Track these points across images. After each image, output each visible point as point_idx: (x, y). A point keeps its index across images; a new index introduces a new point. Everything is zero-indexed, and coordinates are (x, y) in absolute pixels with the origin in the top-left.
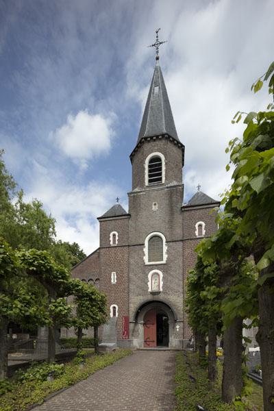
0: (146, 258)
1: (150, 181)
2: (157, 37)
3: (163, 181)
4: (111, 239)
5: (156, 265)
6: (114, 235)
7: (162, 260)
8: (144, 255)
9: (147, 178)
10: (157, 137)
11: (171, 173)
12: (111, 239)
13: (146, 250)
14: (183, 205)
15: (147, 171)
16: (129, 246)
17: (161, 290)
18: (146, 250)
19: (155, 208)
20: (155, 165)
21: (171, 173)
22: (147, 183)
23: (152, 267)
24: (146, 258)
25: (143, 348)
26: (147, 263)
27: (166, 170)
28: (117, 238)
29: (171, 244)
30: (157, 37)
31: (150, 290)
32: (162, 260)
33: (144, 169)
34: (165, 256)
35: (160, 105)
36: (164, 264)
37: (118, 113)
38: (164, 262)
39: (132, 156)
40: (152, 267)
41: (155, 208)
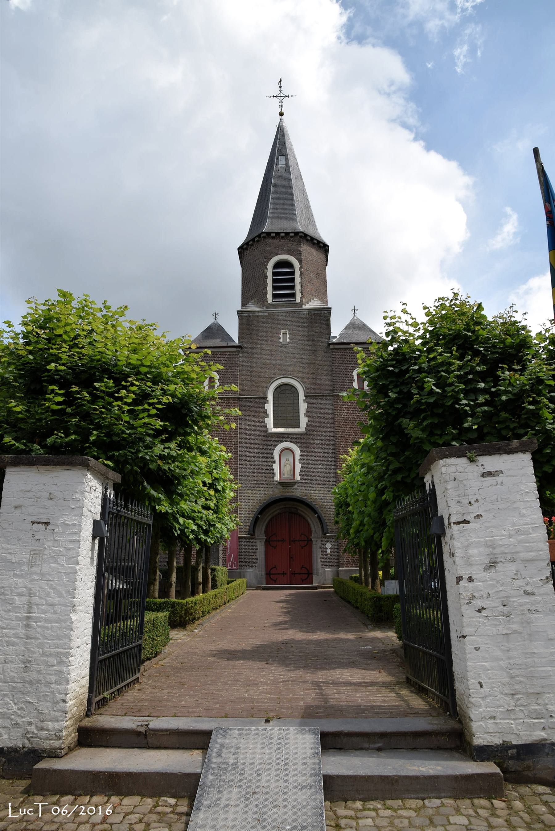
1: (275, 296)
7: (298, 426)
8: (267, 415)
10: (287, 234)
13: (270, 407)
16: (239, 398)
17: (298, 478)
18: (270, 407)
20: (284, 278)
23: (282, 437)
24: (270, 421)
29: (313, 400)
30: (281, 87)
31: (277, 478)
32: (298, 426)
33: (266, 277)
34: (304, 421)
36: (302, 434)
38: (301, 429)
40: (282, 437)
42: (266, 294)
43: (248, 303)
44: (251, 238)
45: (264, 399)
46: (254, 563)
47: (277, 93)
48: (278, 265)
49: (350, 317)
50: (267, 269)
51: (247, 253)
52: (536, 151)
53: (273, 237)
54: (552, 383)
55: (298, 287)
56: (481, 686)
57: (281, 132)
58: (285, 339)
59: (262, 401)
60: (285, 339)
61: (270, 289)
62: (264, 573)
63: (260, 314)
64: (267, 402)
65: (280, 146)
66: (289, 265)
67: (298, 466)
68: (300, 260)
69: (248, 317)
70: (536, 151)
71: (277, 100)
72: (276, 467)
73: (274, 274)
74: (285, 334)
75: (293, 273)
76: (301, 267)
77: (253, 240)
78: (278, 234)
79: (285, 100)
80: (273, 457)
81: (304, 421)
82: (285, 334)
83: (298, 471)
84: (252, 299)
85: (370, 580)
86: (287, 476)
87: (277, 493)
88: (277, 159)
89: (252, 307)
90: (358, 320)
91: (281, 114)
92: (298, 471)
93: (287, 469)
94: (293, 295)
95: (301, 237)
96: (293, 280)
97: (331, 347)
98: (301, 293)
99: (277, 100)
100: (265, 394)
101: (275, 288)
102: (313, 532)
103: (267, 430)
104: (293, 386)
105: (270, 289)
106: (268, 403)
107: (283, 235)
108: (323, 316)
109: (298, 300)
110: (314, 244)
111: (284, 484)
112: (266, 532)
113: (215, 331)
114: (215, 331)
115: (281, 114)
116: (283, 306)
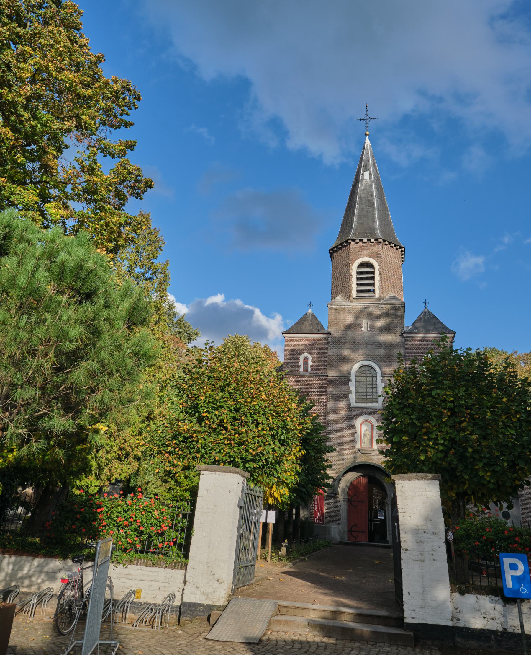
0: (352, 397)
2: (367, 111)
3: (377, 294)
4: (301, 363)
5: (368, 409)
6: (306, 359)
8: (350, 392)
9: (354, 287)
11: (387, 283)
12: (301, 363)
14: (405, 329)
15: (354, 281)
19: (506, 240)
21: (387, 283)
22: (354, 293)
24: (352, 397)
25: (346, 540)
26: (354, 404)
27: (381, 282)
28: (310, 364)
30: (367, 111)
33: (349, 275)
35: (372, 196)
37: (190, 492)
39: (332, 252)
41: (506, 240)
43: (336, 296)
46: (338, 520)
47: (363, 116)
48: (362, 265)
49: (422, 309)
50: (352, 269)
51: (335, 254)
56: (409, 594)
59: (346, 379)
61: (354, 281)
62: (346, 529)
63: (346, 307)
64: (350, 380)
66: (370, 265)
68: (379, 262)
71: (363, 123)
75: (373, 273)
76: (380, 268)
84: (340, 293)
85: (343, 579)
88: (363, 174)
90: (429, 312)
94: (374, 291)
97: (405, 335)
98: (380, 289)
102: (389, 495)
104: (372, 368)
105: (354, 281)
106: (351, 381)
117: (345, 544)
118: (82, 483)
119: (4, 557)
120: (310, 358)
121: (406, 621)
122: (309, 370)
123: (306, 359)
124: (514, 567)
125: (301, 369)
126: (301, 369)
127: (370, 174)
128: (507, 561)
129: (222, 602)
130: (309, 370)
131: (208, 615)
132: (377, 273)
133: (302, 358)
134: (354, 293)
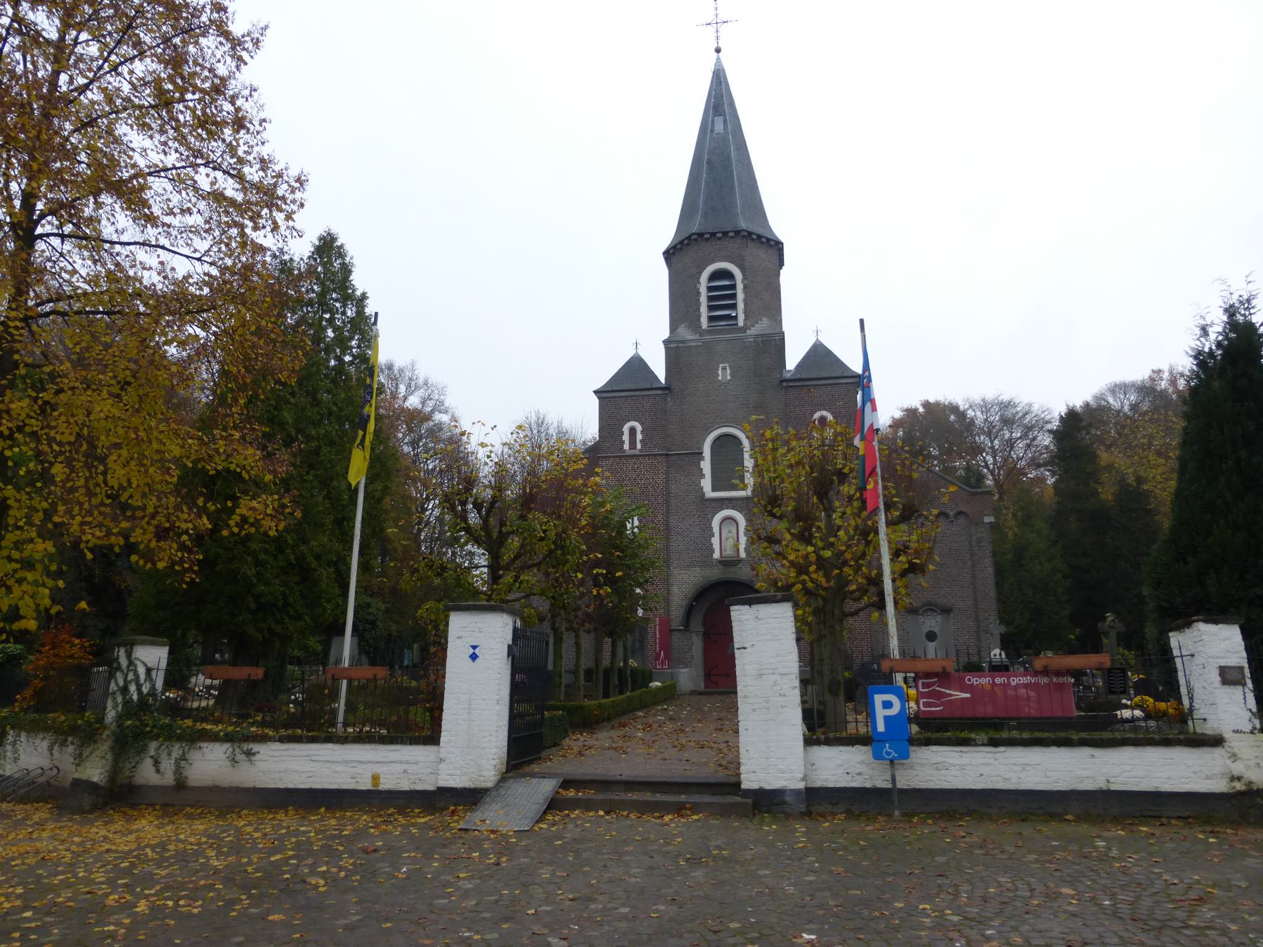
1: (711, 319)
4: (626, 437)
5: (731, 500)
6: (633, 431)
7: (426, 729)
8: (703, 476)
12: (626, 437)
13: (706, 465)
17: (743, 555)
18: (706, 465)
20: (722, 295)
22: (704, 322)
24: (706, 484)
25: (702, 687)
28: (639, 437)
31: (716, 555)
32: (426, 729)
33: (699, 293)
34: (750, 480)
36: (747, 499)
38: (748, 492)
42: (699, 316)
44: (680, 239)
45: (699, 455)
47: (711, 18)
52: (862, 321)
53: (707, 239)
54: (4, 806)
55: (741, 306)
57: (719, 81)
58: (724, 375)
60: (724, 375)
61: (704, 310)
62: (701, 673)
64: (703, 459)
65: (720, 103)
66: (728, 275)
67: (743, 540)
69: (677, 348)
70: (862, 321)
71: (712, 29)
72: (715, 541)
73: (710, 289)
74: (724, 369)
75: (733, 287)
77: (681, 242)
78: (713, 234)
79: (723, 28)
80: (711, 528)
81: (750, 480)
82: (724, 369)
83: (742, 547)
86: (729, 552)
87: (716, 574)
89: (685, 333)
91: (718, 50)
92: (742, 547)
93: (729, 544)
94: (736, 318)
95: (743, 237)
96: (734, 296)
98: (746, 313)
99: (712, 29)
100: (701, 448)
101: (711, 308)
103: (704, 494)
105: (704, 310)
107: (719, 235)
108: (776, 343)
109: (741, 323)
110: (762, 243)
111: (726, 563)
112: (705, 623)
113: (636, 366)
114: (636, 366)
115: (718, 50)
116: (721, 332)
117: (700, 693)
118: (31, 16)
119: (804, 779)
120: (639, 427)
121: (744, 786)
122: (639, 446)
123: (633, 431)
124: (887, 705)
125: (626, 446)
126: (626, 446)
127: (725, 121)
128: (879, 699)
129: (490, 785)
130: (639, 446)
131: (471, 797)
132: (740, 287)
133: (626, 429)
134: (704, 322)
